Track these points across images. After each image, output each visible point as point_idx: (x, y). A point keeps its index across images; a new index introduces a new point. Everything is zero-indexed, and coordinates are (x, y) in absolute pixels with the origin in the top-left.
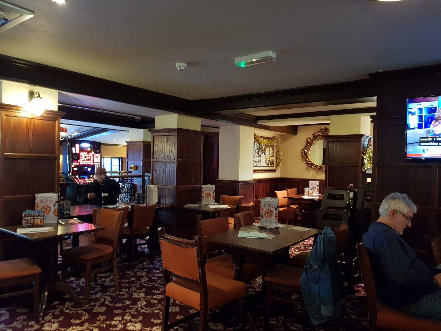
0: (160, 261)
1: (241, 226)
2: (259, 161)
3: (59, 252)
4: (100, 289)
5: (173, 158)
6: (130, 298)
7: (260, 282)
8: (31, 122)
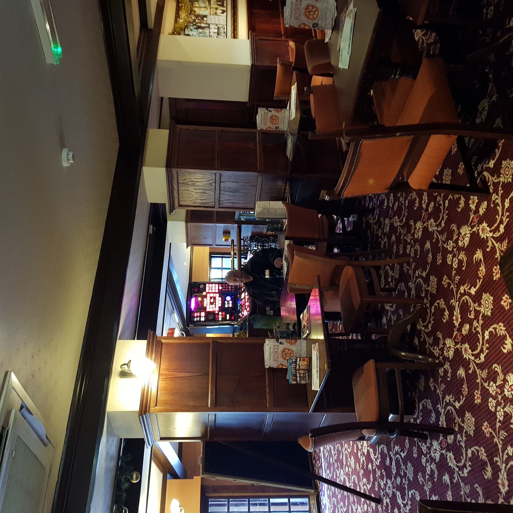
0: (371, 199)
1: (330, 63)
2: (217, 27)
3: (345, 337)
4: (403, 283)
5: (214, 177)
6: (422, 242)
7: (421, 34)
8: (165, 375)
